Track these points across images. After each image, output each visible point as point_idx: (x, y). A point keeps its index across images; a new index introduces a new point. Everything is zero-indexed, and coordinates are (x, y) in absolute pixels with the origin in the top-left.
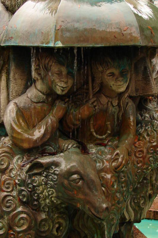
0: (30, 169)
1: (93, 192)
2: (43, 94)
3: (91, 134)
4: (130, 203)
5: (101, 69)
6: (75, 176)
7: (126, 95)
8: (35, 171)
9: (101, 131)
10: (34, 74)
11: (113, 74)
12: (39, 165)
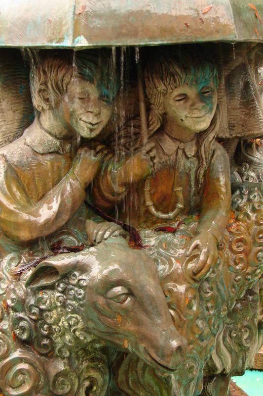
0: (35, 278)
1: (151, 319)
2: (56, 137)
3: (148, 211)
4: (224, 338)
5: (161, 87)
6: (118, 290)
7: (212, 136)
8: (44, 282)
9: (165, 204)
10: (37, 101)
11: (184, 97)
12: (50, 271)
